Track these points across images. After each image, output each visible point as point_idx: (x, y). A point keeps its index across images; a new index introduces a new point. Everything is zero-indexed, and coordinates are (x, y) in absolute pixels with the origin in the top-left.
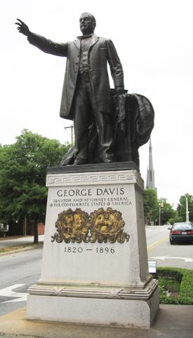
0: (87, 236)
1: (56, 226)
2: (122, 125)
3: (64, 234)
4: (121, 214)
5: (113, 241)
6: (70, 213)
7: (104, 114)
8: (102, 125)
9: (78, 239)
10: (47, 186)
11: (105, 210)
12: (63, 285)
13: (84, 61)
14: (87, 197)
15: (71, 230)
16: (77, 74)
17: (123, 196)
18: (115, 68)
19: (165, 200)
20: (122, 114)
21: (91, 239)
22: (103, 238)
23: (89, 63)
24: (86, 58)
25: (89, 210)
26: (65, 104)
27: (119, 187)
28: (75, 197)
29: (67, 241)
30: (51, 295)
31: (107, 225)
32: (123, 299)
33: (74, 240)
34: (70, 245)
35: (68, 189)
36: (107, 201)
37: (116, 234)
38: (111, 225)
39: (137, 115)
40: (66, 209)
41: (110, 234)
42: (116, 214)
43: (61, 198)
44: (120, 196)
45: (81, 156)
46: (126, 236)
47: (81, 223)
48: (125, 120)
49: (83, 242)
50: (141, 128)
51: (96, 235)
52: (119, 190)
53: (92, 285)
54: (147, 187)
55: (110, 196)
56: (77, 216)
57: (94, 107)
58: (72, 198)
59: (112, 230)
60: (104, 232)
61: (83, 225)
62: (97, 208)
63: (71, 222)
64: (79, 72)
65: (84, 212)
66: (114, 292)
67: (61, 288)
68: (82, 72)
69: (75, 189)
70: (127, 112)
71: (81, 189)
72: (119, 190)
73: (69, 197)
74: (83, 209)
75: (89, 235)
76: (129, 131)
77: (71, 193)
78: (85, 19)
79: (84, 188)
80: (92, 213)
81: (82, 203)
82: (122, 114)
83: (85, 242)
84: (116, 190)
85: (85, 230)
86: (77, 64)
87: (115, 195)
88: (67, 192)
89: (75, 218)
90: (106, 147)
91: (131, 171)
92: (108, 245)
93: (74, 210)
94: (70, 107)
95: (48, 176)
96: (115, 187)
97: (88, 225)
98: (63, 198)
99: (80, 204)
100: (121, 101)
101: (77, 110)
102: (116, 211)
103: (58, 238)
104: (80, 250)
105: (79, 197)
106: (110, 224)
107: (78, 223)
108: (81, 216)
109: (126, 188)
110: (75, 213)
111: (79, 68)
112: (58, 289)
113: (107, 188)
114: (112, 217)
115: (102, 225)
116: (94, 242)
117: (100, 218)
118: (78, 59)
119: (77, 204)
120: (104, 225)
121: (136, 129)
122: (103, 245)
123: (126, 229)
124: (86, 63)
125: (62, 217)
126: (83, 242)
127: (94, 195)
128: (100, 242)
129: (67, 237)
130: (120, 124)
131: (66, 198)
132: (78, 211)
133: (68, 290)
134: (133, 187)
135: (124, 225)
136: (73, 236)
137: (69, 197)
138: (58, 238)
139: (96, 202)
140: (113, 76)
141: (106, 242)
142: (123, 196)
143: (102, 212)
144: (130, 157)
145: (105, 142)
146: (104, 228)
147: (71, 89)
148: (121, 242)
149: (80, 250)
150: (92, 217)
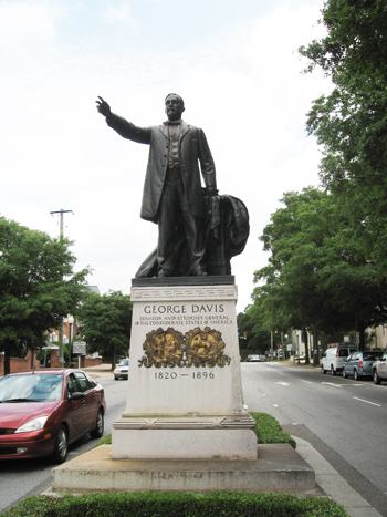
0: (181, 359)
5: (212, 364)
6: (160, 332)
7: (196, 218)
9: (171, 362)
11: (202, 329)
13: (175, 154)
15: (162, 352)
16: (165, 168)
20: (215, 220)
22: (200, 362)
25: (183, 329)
27: (218, 304)
28: (166, 314)
29: (158, 366)
31: (205, 347)
32: (226, 428)
33: (167, 364)
36: (204, 320)
40: (156, 328)
43: (148, 315)
46: (227, 359)
48: (219, 227)
52: (218, 308)
53: (190, 415)
55: (208, 314)
56: (169, 337)
59: (212, 352)
61: (177, 347)
62: (192, 327)
63: (163, 344)
65: (177, 332)
66: (217, 421)
71: (173, 305)
73: (158, 314)
74: (176, 328)
75: (184, 358)
77: (162, 309)
78: (174, 101)
79: (178, 304)
82: (215, 220)
83: (180, 366)
85: (179, 352)
87: (213, 313)
92: (207, 369)
93: (165, 329)
97: (183, 346)
98: (152, 315)
102: (214, 331)
103: (147, 362)
105: (170, 315)
106: (208, 345)
108: (174, 336)
110: (166, 332)
112: (151, 422)
114: (210, 337)
115: (199, 346)
116: (190, 366)
122: (201, 369)
123: (226, 351)
125: (151, 338)
127: (189, 312)
128: (197, 366)
129: (158, 360)
132: (170, 330)
133: (161, 421)
137: (158, 314)
138: (147, 362)
140: (204, 173)
142: (222, 314)
143: (199, 332)
146: (201, 350)
148: (221, 366)
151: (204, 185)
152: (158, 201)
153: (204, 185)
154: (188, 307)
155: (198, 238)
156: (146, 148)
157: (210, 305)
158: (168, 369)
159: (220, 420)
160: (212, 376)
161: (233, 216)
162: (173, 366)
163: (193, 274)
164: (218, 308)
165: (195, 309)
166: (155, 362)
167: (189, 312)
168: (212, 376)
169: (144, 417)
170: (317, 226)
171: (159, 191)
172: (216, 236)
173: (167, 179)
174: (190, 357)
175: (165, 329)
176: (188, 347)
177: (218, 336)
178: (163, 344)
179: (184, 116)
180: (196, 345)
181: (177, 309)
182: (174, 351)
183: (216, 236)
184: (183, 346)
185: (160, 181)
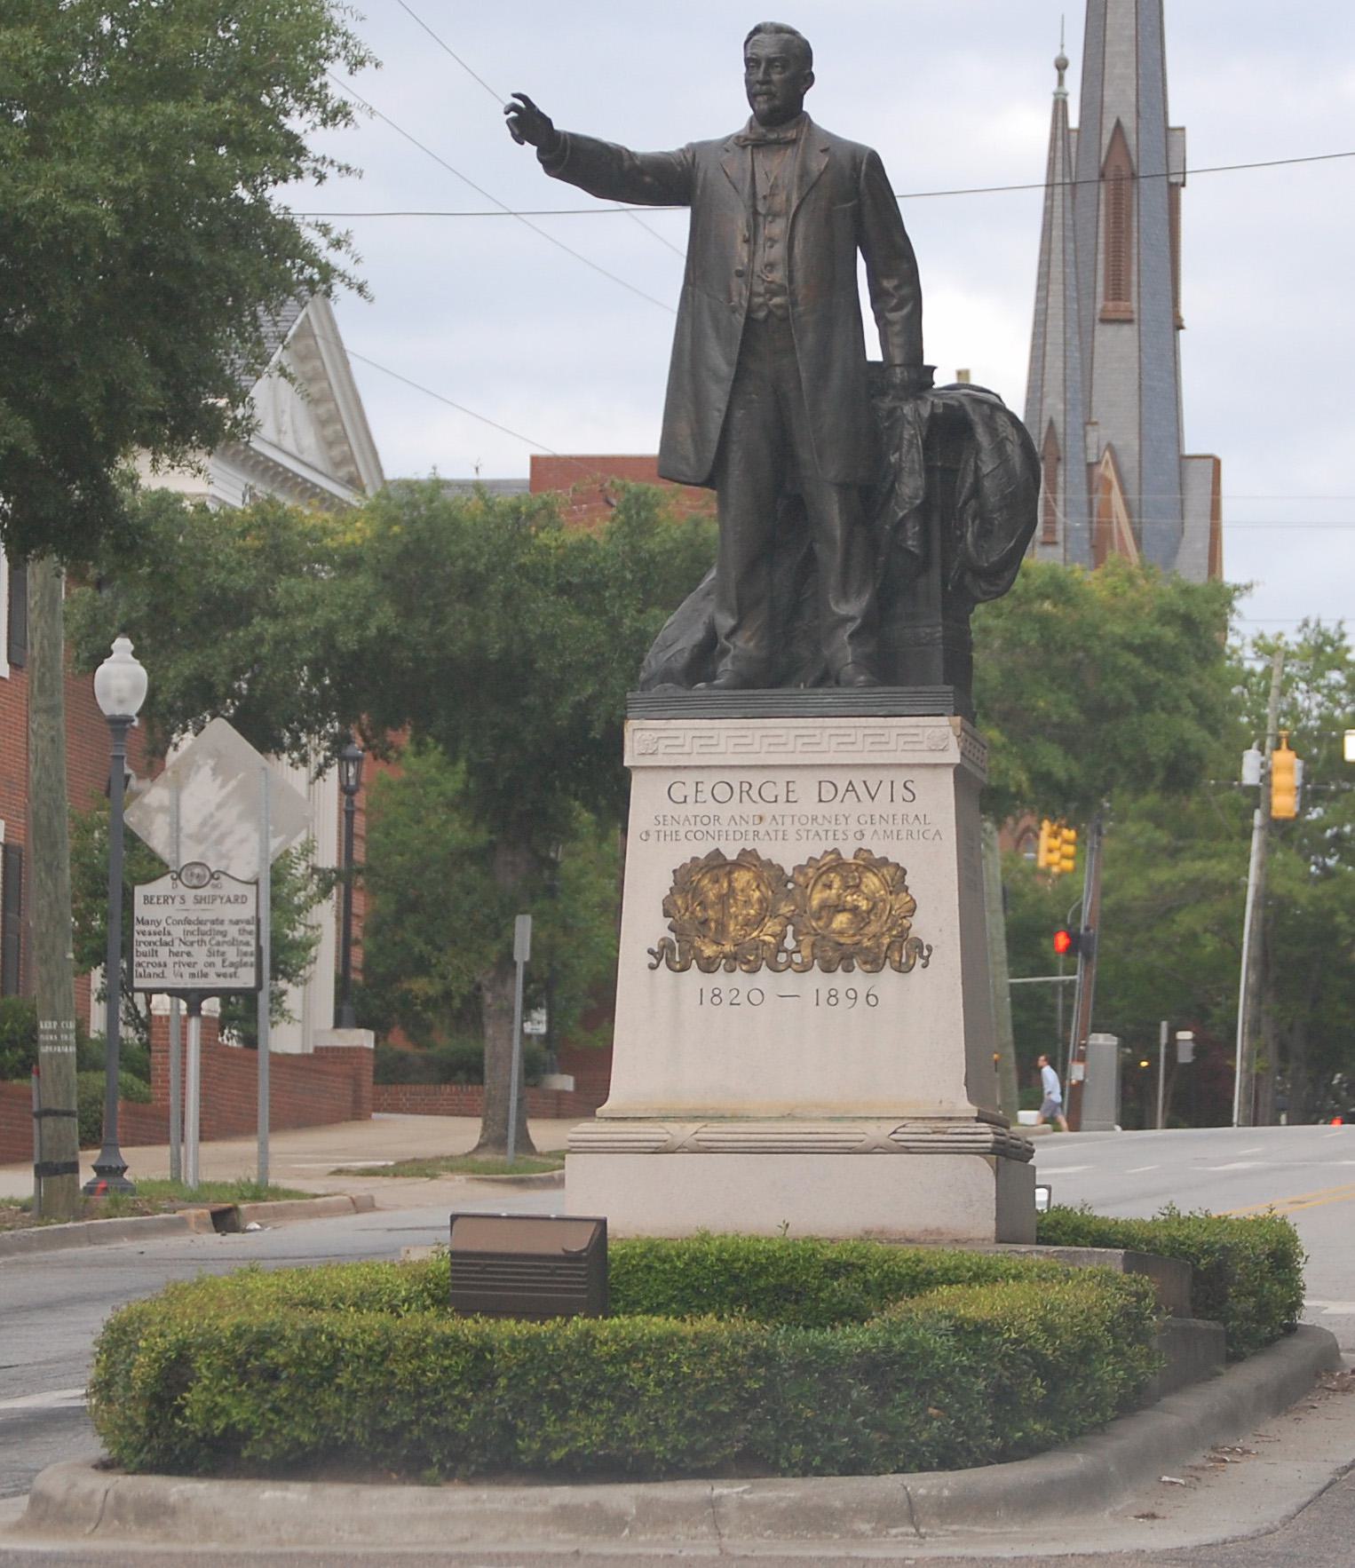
0: (779, 948)
1: (667, 914)
2: (912, 529)
3: (698, 942)
4: (905, 872)
5: (874, 964)
6: (716, 864)
7: (843, 488)
8: (838, 533)
9: (746, 958)
10: (626, 764)
11: (848, 856)
12: (696, 1118)
13: (771, 266)
14: (781, 807)
15: (722, 927)
16: (740, 319)
17: (912, 810)
18: (888, 284)
19: (286, 208)
20: (911, 487)
21: (797, 958)
22: (837, 957)
23: (791, 279)
24: (778, 251)
25: (788, 854)
26: (684, 429)
27: (900, 777)
28: (733, 808)
29: (708, 967)
30: (657, 1151)
31: (855, 910)
32: (908, 1151)
33: (734, 960)
34: (720, 979)
35: (709, 779)
36: (853, 826)
37: (886, 941)
38: (869, 912)
39: (970, 480)
40: (702, 850)
41: (866, 943)
42: (887, 872)
43: (681, 811)
44: (900, 808)
45: (745, 644)
46: (920, 949)
47: (760, 901)
48: (924, 511)
49: (764, 970)
50: (984, 534)
51: (813, 945)
52: (898, 786)
54: (1087, 929)
55: (867, 806)
56: (742, 878)
57: (804, 454)
58: (726, 812)
59: (873, 928)
60: (841, 933)
61: (767, 910)
63: (723, 899)
64: (750, 311)
65: (769, 864)
66: (877, 1132)
67: (692, 1127)
68: (761, 314)
69: (734, 778)
70: (929, 470)
71: (756, 779)
72: (898, 786)
73: (712, 808)
74: (766, 851)
75: (790, 943)
76: (936, 546)
77: (723, 793)
78: (768, 47)
79: (681, 776)
80: (799, 869)
81: (762, 828)
82: (911, 487)
83: (774, 968)
84: (886, 787)
85: (771, 926)
86: (740, 274)
87: (882, 805)
88: (706, 788)
89: (738, 885)
90: (850, 619)
91: (944, 720)
92: (858, 979)
93: (732, 856)
94: (711, 454)
95: (631, 726)
96: (886, 775)
97: (786, 909)
98: (690, 809)
99: (756, 833)
100: (908, 433)
101: (736, 455)
102: (884, 862)
104: (756, 997)
105: (750, 809)
106: (864, 905)
107: (747, 903)
108: (758, 878)
109: (921, 780)
110: (737, 865)
111: (752, 294)
113: (857, 778)
114: (871, 882)
115: (838, 908)
116: (805, 968)
117: (830, 887)
118: (742, 251)
119: (744, 835)
120: (844, 910)
121: (963, 537)
122: (839, 979)
123: (921, 926)
124: (778, 276)
125: (686, 881)
126: (764, 970)
127: (807, 802)
128: (828, 969)
129: (709, 951)
130: (900, 525)
131: (700, 810)
132: (748, 859)
133: (714, 1131)
134: (948, 778)
135: (913, 910)
136: (728, 948)
137: (712, 808)
138: (666, 955)
139: (815, 827)
140: (879, 319)
141: (848, 970)
142: (912, 810)
143: (836, 864)
144: (937, 664)
145: (844, 595)
146: (841, 920)
147: (719, 410)
148: (903, 968)
149: (756, 997)
150: (801, 880)
151: (874, 352)
152: (714, 433)
153: (874, 352)
154: (806, 786)
155: (847, 553)
156: (675, 222)
157: (873, 778)
158: (739, 976)
159: (893, 1126)
160: (872, 999)
161: (977, 469)
162: (754, 970)
163: (827, 678)
164: (899, 791)
165: (828, 792)
166: (698, 956)
167: (807, 802)
168: (872, 999)
169: (665, 1118)
170: (334, 891)
171: (718, 396)
172: (911, 543)
173: (747, 348)
174: (807, 940)
175: (732, 856)
176: (802, 910)
177: (897, 880)
178: (723, 899)
179: (814, 104)
180: (824, 906)
181: (768, 793)
182: (759, 922)
183: (911, 543)
184: (786, 909)
185: (720, 360)
